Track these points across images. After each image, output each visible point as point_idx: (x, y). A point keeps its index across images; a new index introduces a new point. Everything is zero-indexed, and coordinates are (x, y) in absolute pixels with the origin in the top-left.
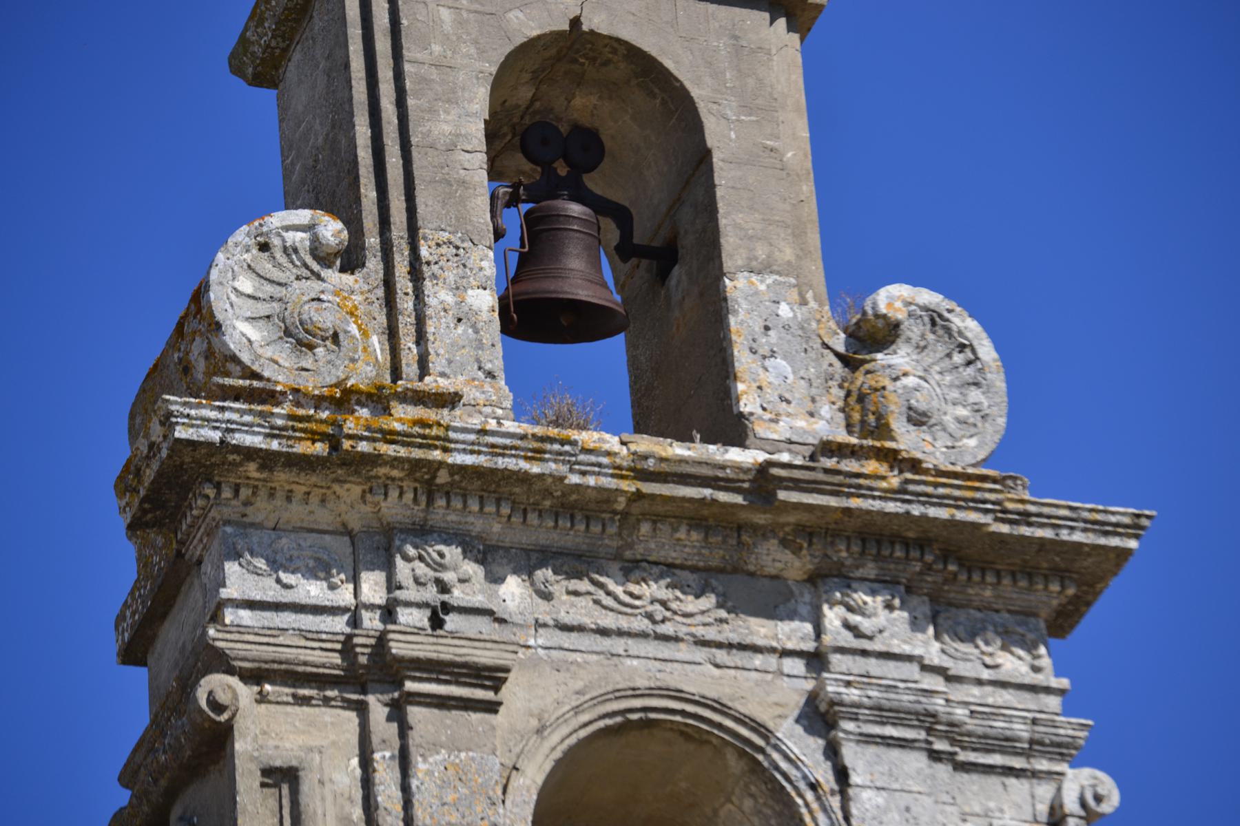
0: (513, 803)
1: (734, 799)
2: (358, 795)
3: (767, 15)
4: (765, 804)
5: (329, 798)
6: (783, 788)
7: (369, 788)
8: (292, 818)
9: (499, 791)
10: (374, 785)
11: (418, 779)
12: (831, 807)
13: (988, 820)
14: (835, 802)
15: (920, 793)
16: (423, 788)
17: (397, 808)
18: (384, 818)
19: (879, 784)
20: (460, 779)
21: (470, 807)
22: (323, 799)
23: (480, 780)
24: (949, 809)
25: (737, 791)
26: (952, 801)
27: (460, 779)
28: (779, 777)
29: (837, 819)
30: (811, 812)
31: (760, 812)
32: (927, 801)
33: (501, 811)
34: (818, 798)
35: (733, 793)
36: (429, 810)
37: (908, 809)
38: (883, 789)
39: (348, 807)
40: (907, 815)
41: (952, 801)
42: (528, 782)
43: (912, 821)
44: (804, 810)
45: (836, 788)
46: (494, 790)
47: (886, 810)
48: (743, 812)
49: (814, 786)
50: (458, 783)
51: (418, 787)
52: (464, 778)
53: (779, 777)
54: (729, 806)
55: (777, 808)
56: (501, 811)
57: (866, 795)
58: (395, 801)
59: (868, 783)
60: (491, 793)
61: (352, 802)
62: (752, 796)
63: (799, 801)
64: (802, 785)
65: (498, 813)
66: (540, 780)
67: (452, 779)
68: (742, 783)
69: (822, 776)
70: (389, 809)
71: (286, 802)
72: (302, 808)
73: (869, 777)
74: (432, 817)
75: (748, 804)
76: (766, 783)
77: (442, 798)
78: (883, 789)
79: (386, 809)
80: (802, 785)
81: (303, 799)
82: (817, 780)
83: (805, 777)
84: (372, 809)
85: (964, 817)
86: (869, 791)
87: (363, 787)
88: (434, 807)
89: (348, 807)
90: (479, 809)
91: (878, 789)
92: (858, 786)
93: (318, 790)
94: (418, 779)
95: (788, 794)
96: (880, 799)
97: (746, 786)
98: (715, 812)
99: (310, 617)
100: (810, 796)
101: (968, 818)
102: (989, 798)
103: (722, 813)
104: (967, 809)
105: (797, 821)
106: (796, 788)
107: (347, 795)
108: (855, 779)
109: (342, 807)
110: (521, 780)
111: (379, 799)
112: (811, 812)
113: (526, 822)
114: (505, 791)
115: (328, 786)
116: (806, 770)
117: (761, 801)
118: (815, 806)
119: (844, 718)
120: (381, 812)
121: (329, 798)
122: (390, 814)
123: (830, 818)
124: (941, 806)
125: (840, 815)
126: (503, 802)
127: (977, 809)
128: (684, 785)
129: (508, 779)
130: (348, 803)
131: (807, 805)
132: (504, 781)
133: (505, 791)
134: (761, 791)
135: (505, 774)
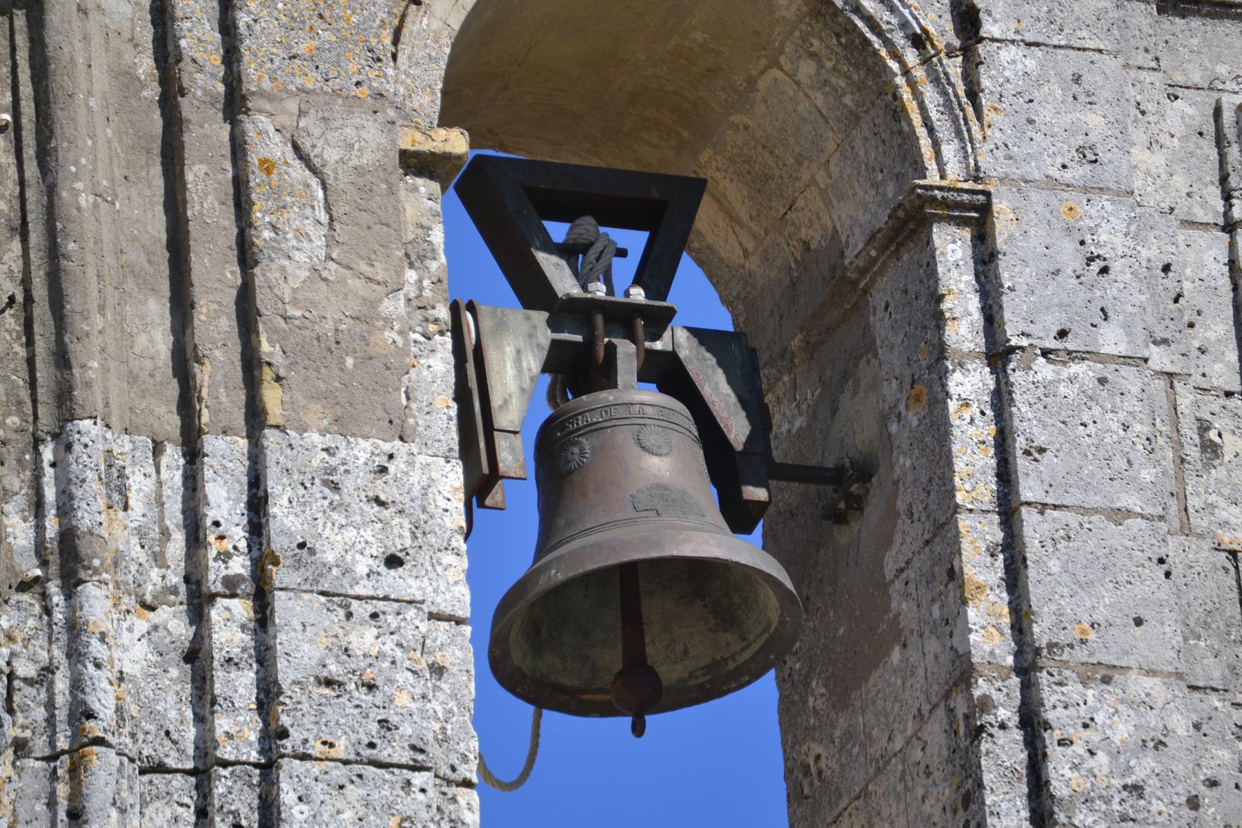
0: (410, 58)
1: (782, 60)
2: (146, 34)
3: (624, 723)
4: (834, 68)
5: (97, 39)
6: (867, 42)
7: (165, 24)
8: (32, 67)
9: (388, 41)
10: (173, 19)
11: (249, 13)
12: (946, 74)
13: (1216, 95)
14: (954, 68)
15: (1100, 51)
16: (257, 27)
17: (214, 60)
18: (190, 74)
19: (1029, 37)
20: (321, 16)
21: (337, 64)
22: (86, 38)
23: (354, 19)
24: (1148, 77)
25: (789, 47)
26: (1153, 64)
27: (321, 16)
28: (860, 24)
29: (956, 95)
30: (912, 84)
31: (826, 82)
32: (1110, 64)
33: (390, 72)
34: (926, 61)
35: (781, 51)
36: (269, 65)
37: (1077, 79)
38: (1037, 44)
39: (128, 55)
40: (1075, 88)
41: (1153, 64)
42: (436, 25)
43: (1082, 98)
44: (900, 81)
45: (957, 43)
46: (377, 36)
47: (1040, 81)
48: (798, 83)
49: (919, 41)
50: (317, 23)
51: (249, 27)
52: (327, 14)
53: (860, 24)
54: (775, 72)
55: (856, 77)
56: (390, 72)
57: (1007, 54)
58: (210, 47)
59: (1011, 36)
60: (374, 41)
61: (136, 46)
62: (813, 55)
63: (894, 66)
64: (899, 39)
65: (385, 76)
66: (456, 22)
67: (306, 13)
68: (797, 33)
69: (932, 22)
70: (201, 62)
71: (21, 40)
72: (50, 52)
73: (1013, 25)
74: (273, 79)
75: (807, 69)
76: (838, 36)
77: (290, 47)
78: (1037, 44)
79: (194, 61)
80: (899, 39)
81: (52, 38)
82: (923, 29)
83: (904, 25)
84: (171, 60)
85: (1171, 90)
86: (1013, 48)
87: (154, 23)
88: (277, 61)
89: (128, 55)
90: (353, 67)
91: (1029, 45)
92: (994, 40)
93: (76, 23)
94: (249, 13)
95: (875, 53)
96: (1031, 62)
97: (804, 39)
98: (751, 82)
99: (24, 133)
100: (911, 57)
101: (1179, 92)
102: (1219, 60)
103: (761, 85)
104: (1179, 78)
105: (890, 97)
106: (888, 43)
107: (126, 35)
108: (989, 28)
109: (119, 54)
110: (425, 21)
111: (183, 43)
112: (912, 84)
113: (433, 93)
114: (396, 41)
115: (93, 14)
116: (906, 12)
117: (829, 65)
118: (919, 73)
119: (940, 219)
120: (186, 65)
121: (97, 39)
122: (201, 70)
123: (944, 93)
124: (1133, 73)
125: (961, 89)
126: (394, 57)
127: (1196, 77)
128: (699, 36)
129: (403, 18)
130: (129, 46)
131: (906, 72)
132: (396, 22)
133: (396, 41)
134: (828, 47)
135: (398, 11)
